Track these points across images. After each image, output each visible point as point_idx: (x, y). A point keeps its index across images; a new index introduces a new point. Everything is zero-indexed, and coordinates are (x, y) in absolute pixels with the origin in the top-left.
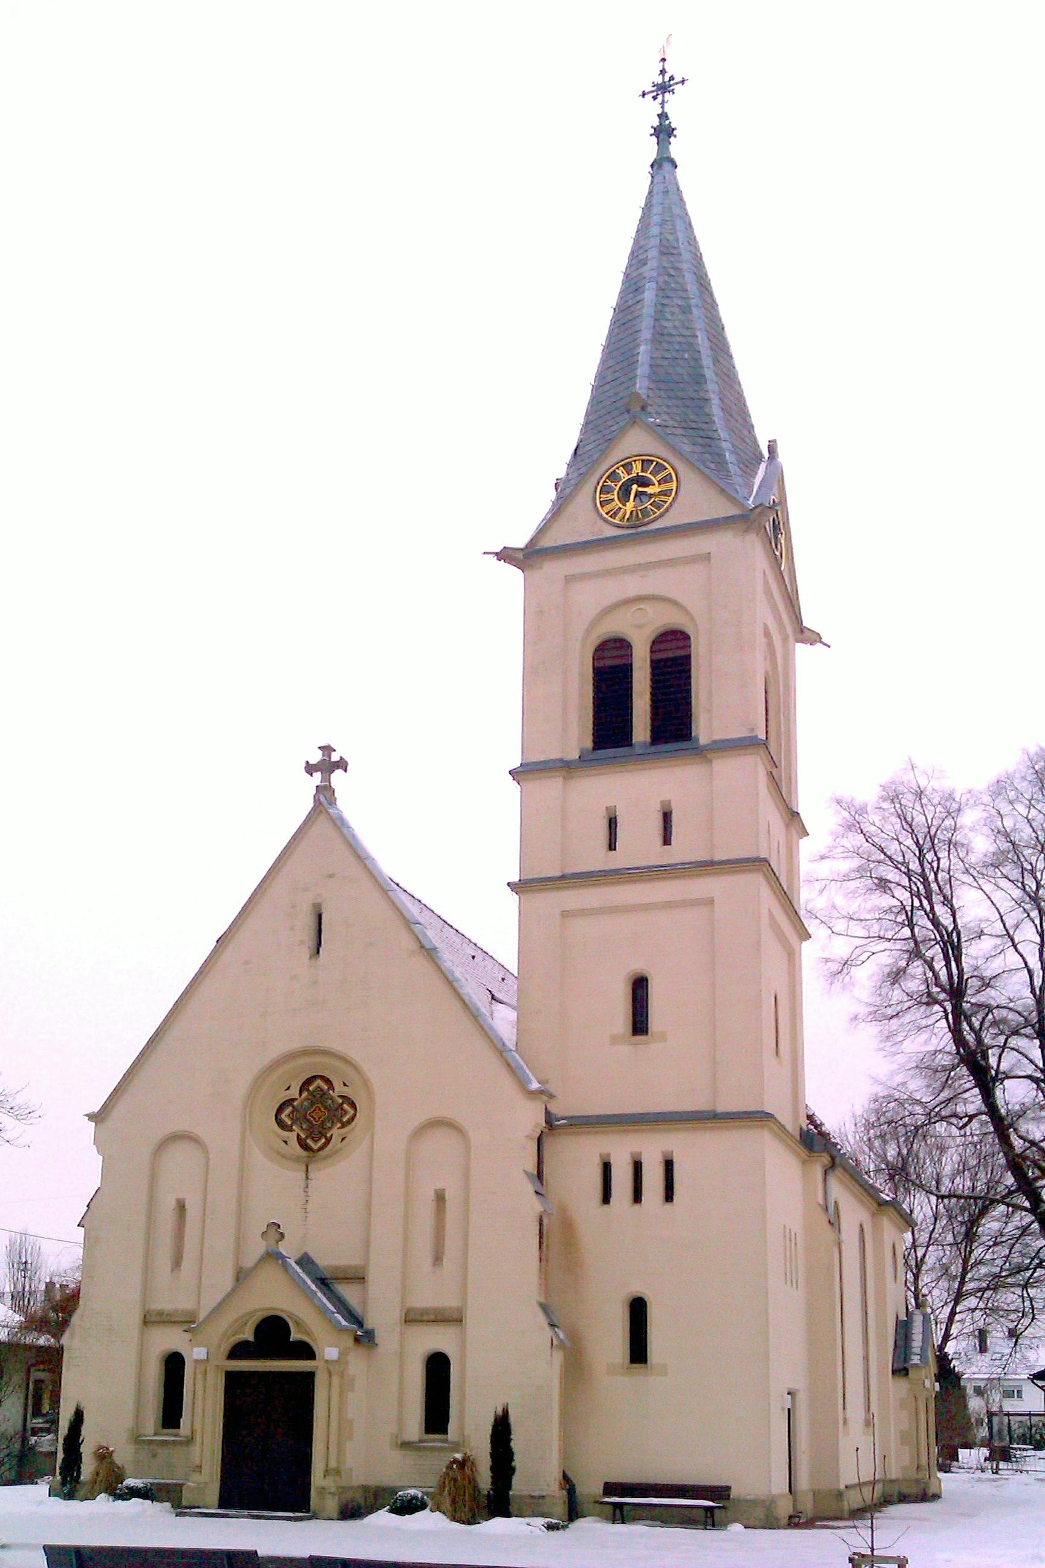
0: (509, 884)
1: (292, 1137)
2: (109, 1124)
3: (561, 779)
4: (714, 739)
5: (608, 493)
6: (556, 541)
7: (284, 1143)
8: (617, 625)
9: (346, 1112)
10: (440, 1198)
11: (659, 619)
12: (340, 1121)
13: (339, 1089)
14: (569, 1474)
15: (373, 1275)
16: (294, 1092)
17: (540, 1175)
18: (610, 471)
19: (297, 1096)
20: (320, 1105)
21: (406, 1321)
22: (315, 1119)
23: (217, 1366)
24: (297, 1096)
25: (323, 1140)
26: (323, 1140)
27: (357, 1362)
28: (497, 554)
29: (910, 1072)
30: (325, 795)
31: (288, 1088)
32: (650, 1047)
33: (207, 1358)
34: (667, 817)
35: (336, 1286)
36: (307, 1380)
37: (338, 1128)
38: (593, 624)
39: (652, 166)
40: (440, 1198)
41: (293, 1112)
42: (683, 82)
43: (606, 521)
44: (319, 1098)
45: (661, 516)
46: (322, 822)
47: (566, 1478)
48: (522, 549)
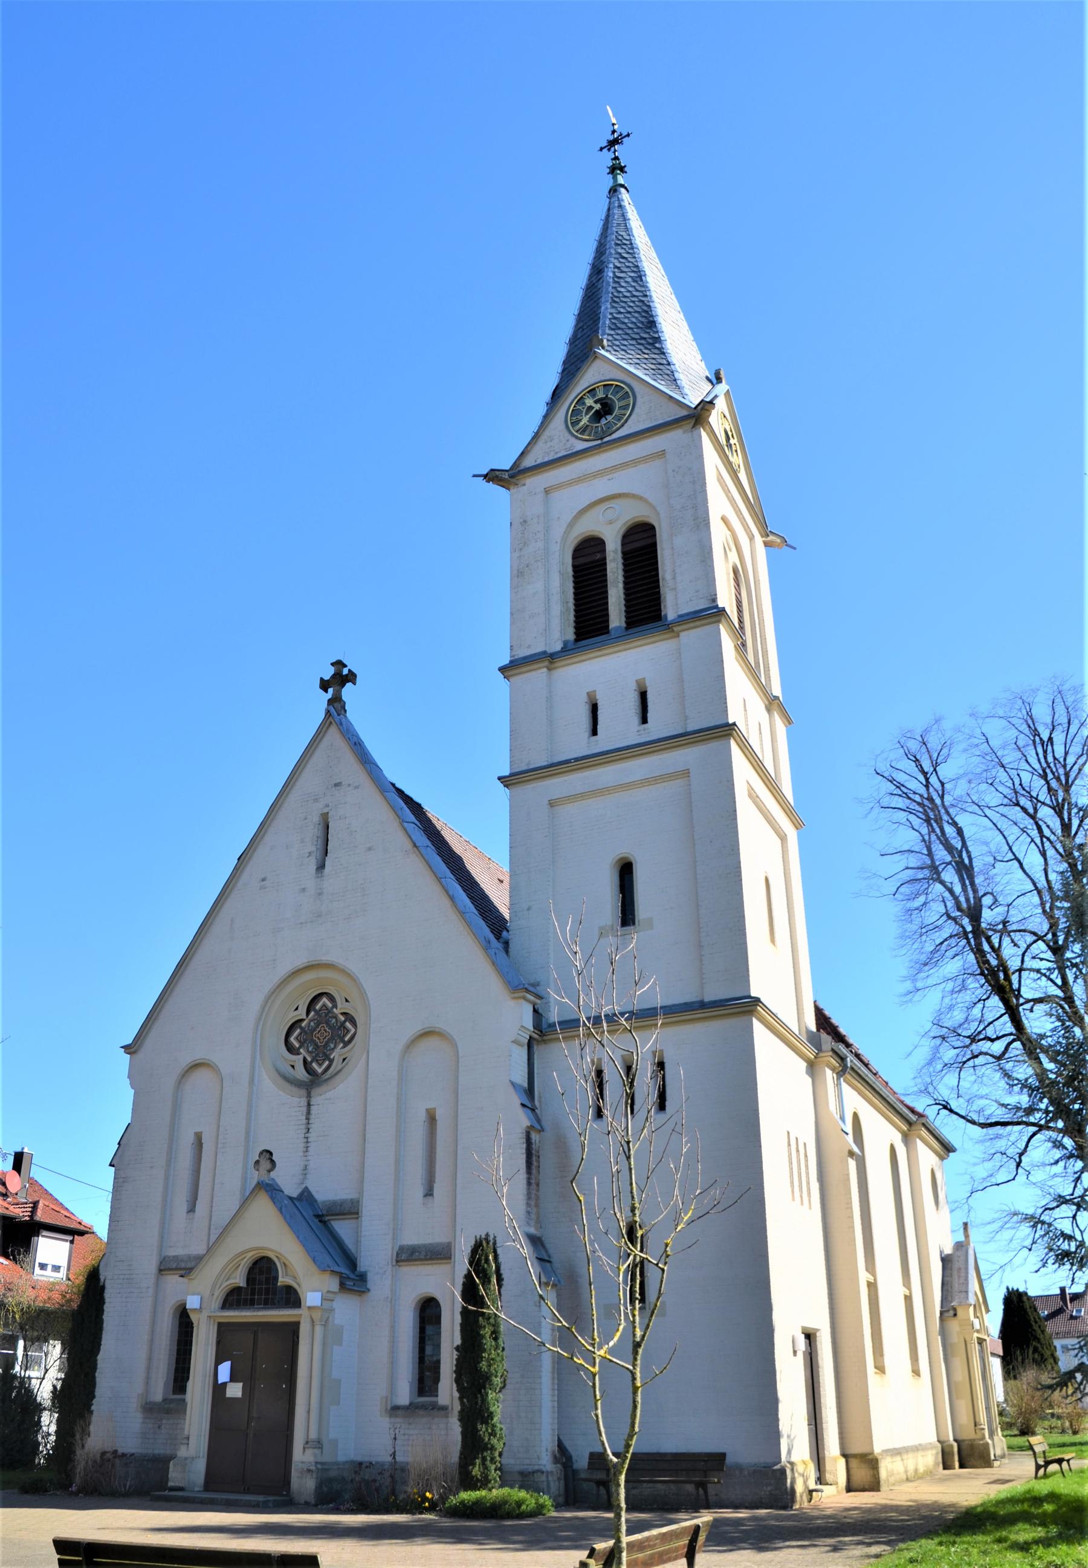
0: (499, 778)
1: (298, 1060)
2: (140, 1055)
3: (545, 670)
4: (679, 613)
5: (577, 415)
6: (536, 461)
7: (291, 1068)
8: (590, 526)
9: (348, 1031)
10: (432, 1118)
11: (628, 514)
12: (343, 1041)
13: (342, 1006)
14: (567, 1444)
15: (368, 1209)
16: (302, 1013)
17: (530, 1091)
18: (578, 398)
19: (304, 1017)
20: (325, 1025)
21: (397, 1261)
22: (319, 1039)
23: (210, 1317)
24: (304, 1017)
25: (327, 1063)
26: (327, 1063)
27: (346, 1309)
28: (485, 476)
29: (903, 903)
30: (336, 702)
31: (297, 1009)
32: (635, 939)
33: (200, 1308)
34: (643, 696)
35: (333, 1223)
36: (292, 1330)
37: (341, 1048)
38: (571, 525)
39: (610, 192)
40: (432, 1118)
41: (300, 1034)
42: (628, 135)
43: (577, 438)
44: (326, 1015)
45: (622, 425)
46: (333, 732)
47: (560, 1445)
48: (507, 471)
